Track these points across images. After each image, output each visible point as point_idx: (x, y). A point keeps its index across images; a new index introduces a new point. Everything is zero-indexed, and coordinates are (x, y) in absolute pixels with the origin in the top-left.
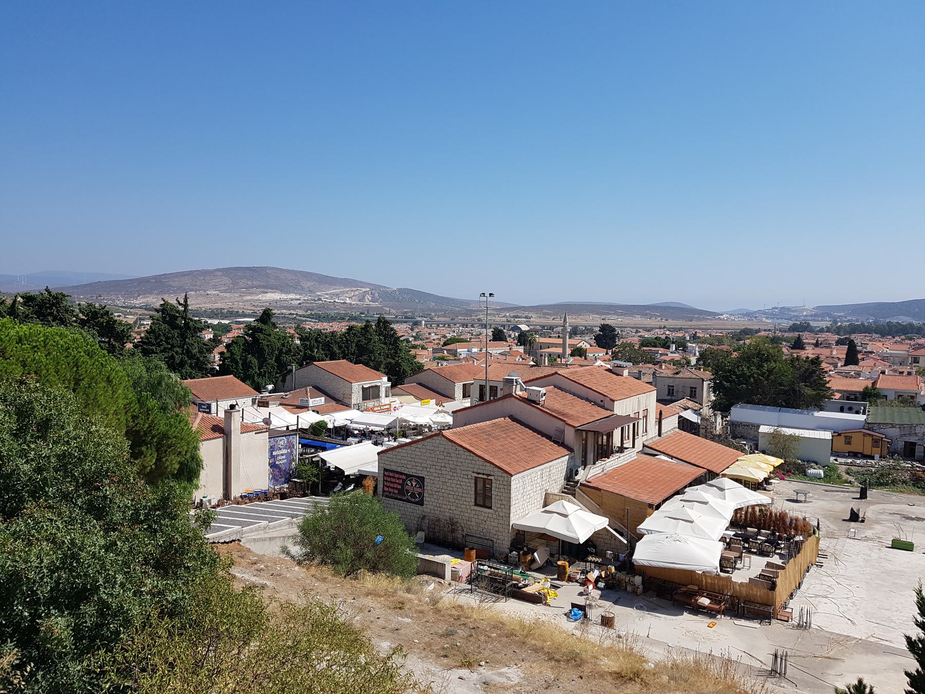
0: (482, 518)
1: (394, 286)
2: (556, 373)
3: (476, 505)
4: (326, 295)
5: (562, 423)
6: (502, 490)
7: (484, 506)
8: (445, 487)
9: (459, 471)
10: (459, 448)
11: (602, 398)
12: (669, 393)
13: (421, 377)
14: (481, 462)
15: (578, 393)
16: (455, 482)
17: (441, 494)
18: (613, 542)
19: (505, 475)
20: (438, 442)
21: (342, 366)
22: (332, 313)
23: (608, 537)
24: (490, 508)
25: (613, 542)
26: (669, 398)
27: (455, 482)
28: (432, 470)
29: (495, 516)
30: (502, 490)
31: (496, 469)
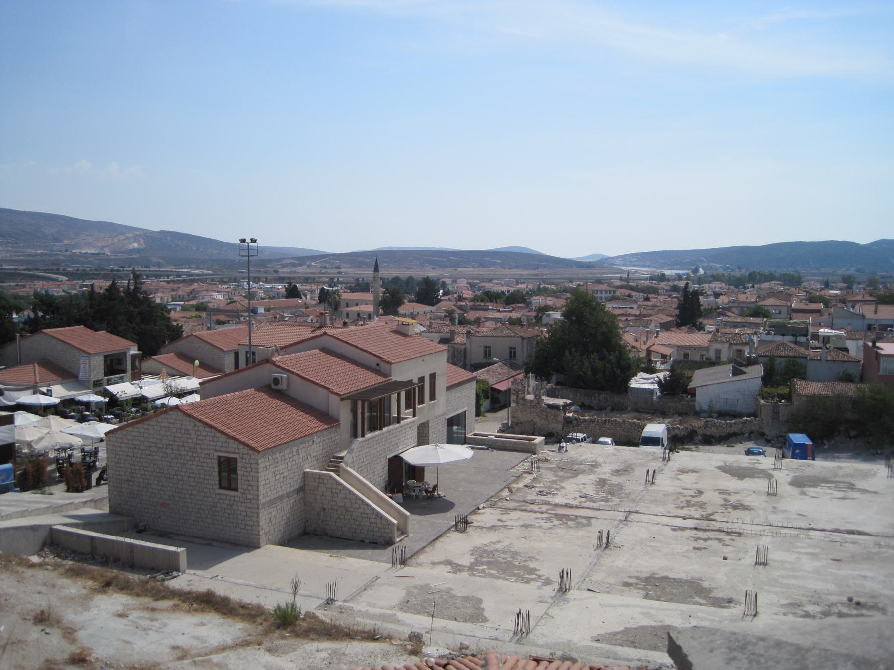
0: (227, 502)
1: (156, 228)
2: (325, 333)
3: (221, 487)
4: (548, 273)
5: (325, 391)
6: (249, 470)
7: (230, 488)
8: (184, 470)
9: (199, 450)
10: (198, 424)
11: (377, 360)
12: (485, 355)
13: (179, 345)
14: (223, 438)
15: (339, 351)
16: (195, 463)
17: (180, 478)
18: (379, 521)
19: (251, 452)
20: (174, 417)
21: (76, 335)
22: (88, 267)
23: (374, 516)
24: (237, 490)
25: (379, 521)
26: (486, 361)
27: (195, 463)
28: (169, 451)
29: (242, 500)
30: (249, 470)
31: (241, 446)
